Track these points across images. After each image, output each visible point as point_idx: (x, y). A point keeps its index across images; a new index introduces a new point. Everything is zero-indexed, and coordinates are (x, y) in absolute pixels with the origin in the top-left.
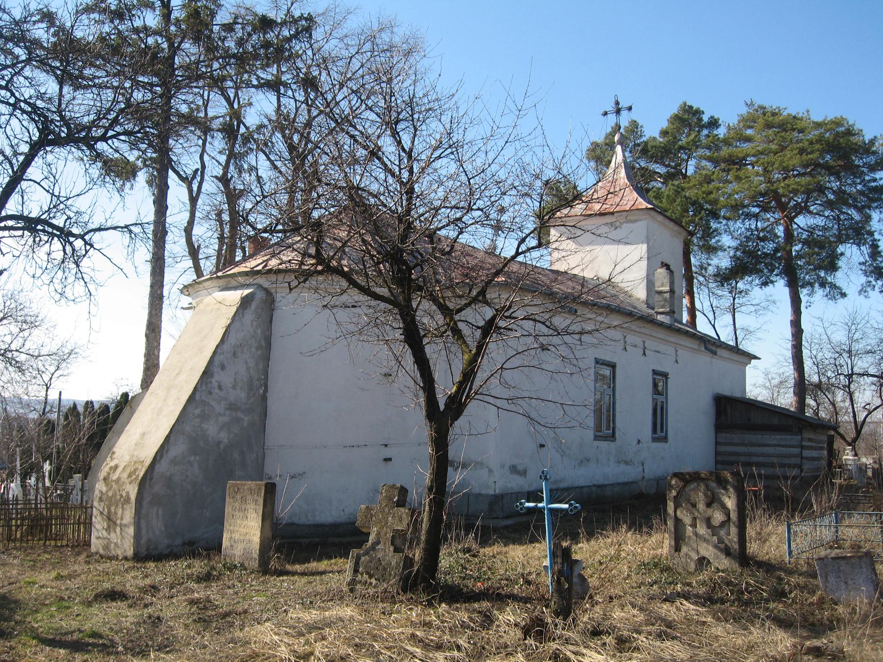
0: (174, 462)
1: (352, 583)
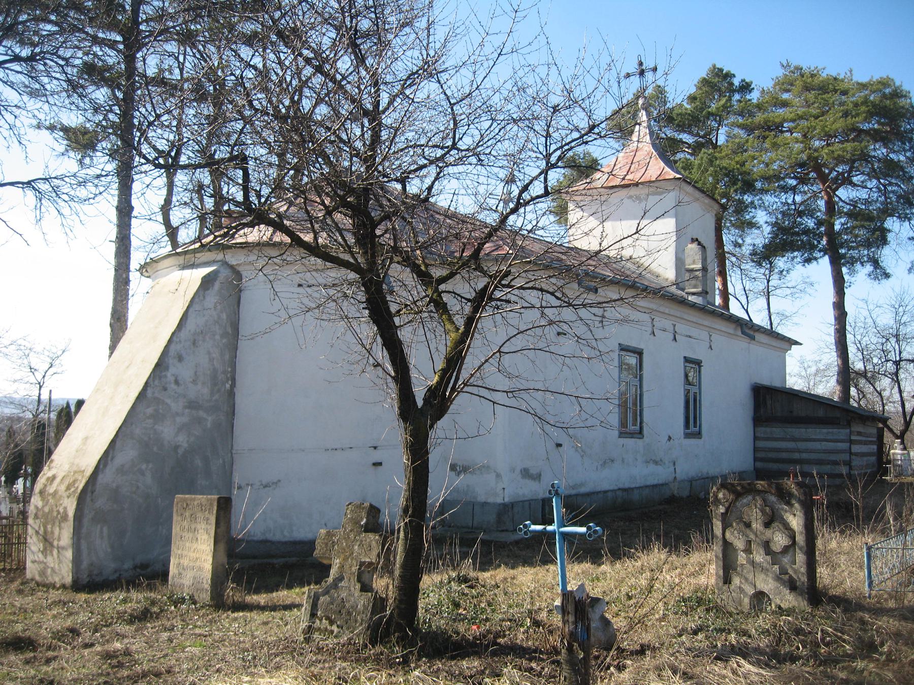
0: (121, 471)
1: (309, 630)
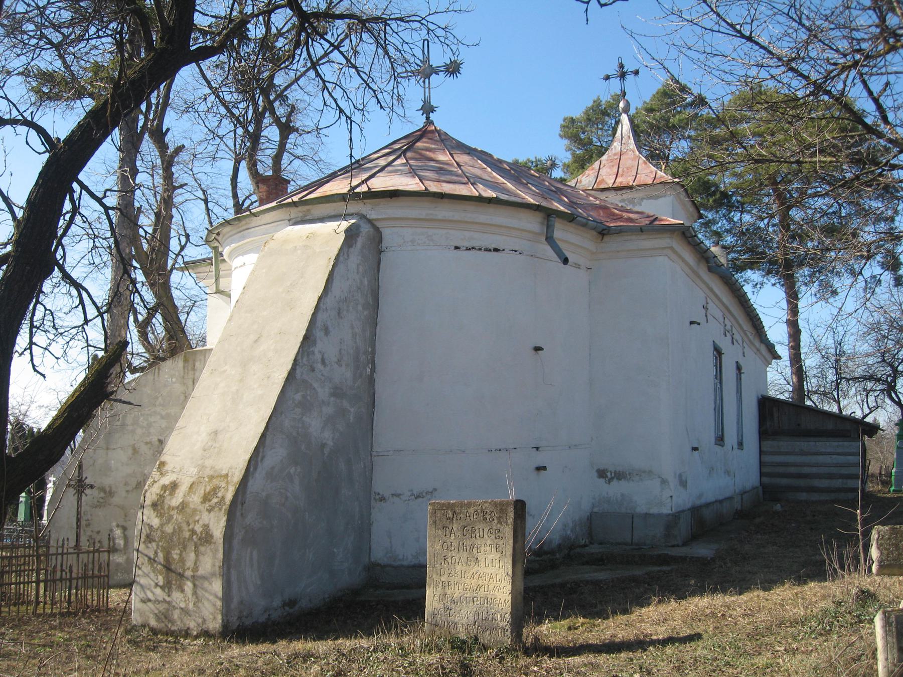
0: (271, 476)
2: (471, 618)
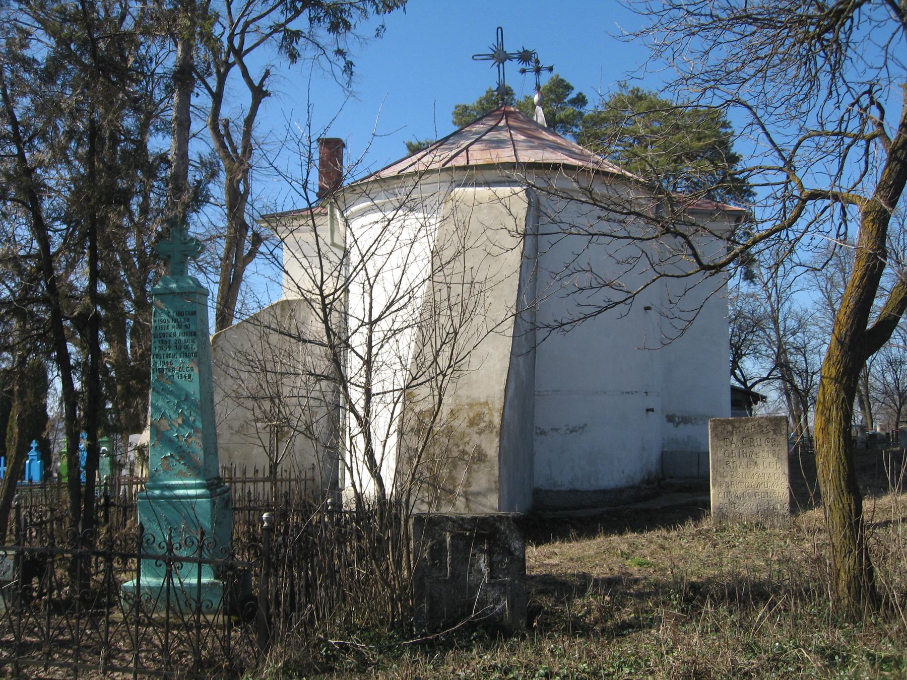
2: (755, 509)
